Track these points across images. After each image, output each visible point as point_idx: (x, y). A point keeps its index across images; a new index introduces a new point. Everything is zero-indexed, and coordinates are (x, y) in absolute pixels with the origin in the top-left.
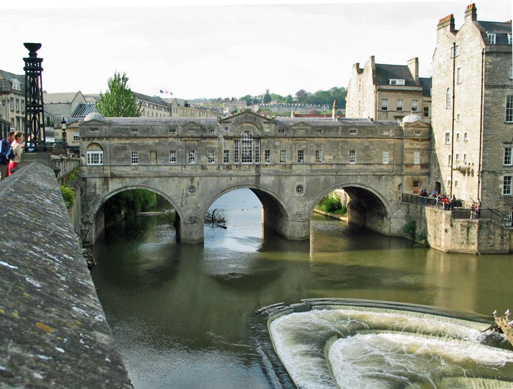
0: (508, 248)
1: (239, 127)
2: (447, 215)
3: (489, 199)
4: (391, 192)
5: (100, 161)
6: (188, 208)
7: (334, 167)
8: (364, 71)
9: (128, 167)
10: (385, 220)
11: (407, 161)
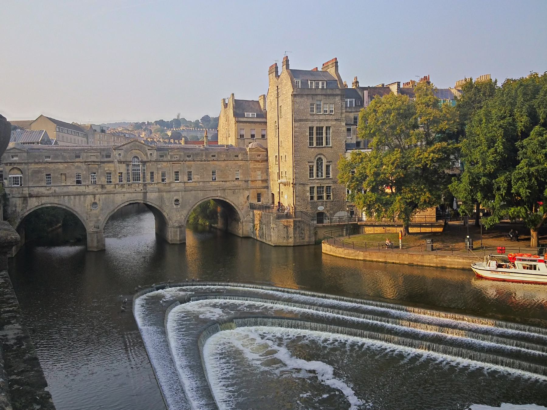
0: (314, 240)
1: (129, 153)
6: (91, 221)
9: (43, 188)
10: (239, 224)
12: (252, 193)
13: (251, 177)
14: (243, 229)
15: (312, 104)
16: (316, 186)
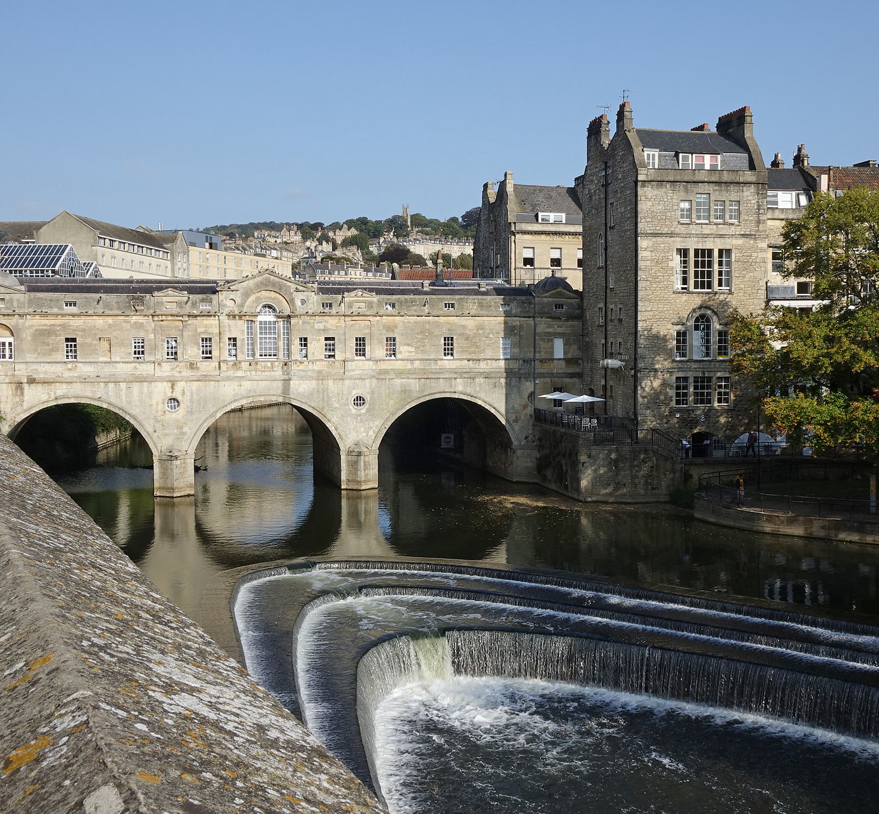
5: (7, 356)
6: (166, 435)
7: (417, 364)
10: (509, 453)
11: (542, 353)
16: (691, 375)
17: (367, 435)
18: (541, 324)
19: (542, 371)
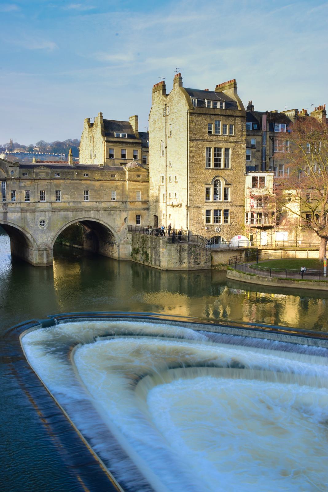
2: (164, 241)
3: (195, 227)
4: (119, 224)
7: (71, 204)
8: (94, 126)
11: (131, 198)
12: (131, 215)
13: (130, 198)
14: (119, 252)
15: (210, 124)
17: (47, 240)
18: (130, 184)
19: (131, 207)
